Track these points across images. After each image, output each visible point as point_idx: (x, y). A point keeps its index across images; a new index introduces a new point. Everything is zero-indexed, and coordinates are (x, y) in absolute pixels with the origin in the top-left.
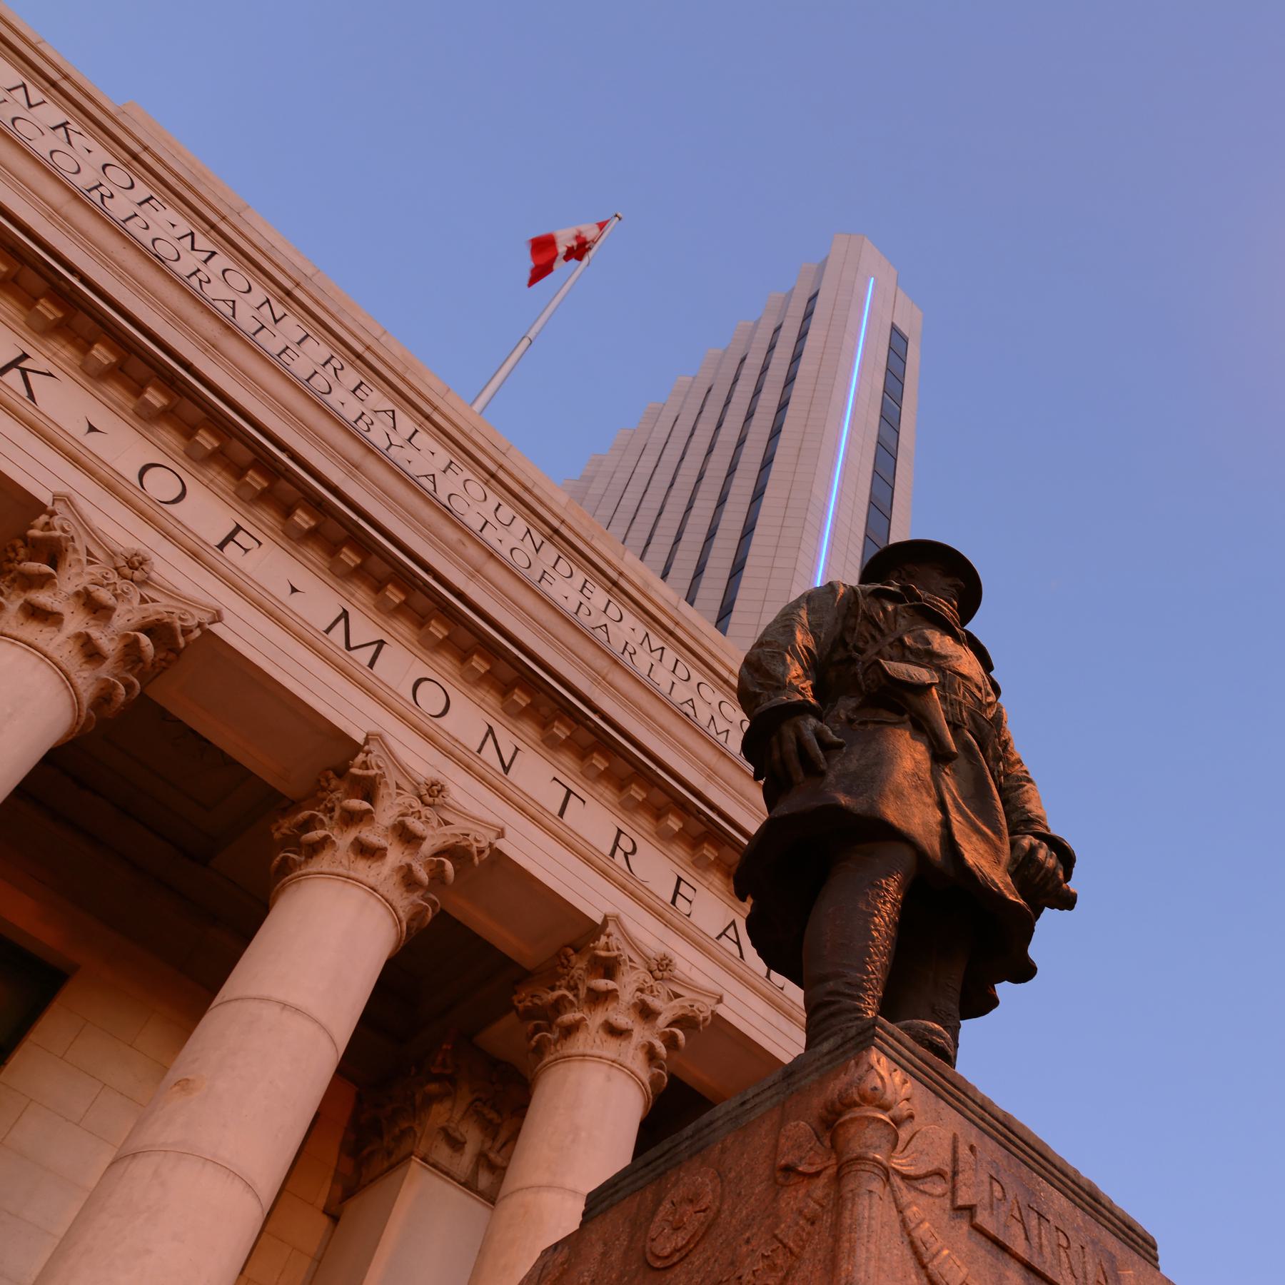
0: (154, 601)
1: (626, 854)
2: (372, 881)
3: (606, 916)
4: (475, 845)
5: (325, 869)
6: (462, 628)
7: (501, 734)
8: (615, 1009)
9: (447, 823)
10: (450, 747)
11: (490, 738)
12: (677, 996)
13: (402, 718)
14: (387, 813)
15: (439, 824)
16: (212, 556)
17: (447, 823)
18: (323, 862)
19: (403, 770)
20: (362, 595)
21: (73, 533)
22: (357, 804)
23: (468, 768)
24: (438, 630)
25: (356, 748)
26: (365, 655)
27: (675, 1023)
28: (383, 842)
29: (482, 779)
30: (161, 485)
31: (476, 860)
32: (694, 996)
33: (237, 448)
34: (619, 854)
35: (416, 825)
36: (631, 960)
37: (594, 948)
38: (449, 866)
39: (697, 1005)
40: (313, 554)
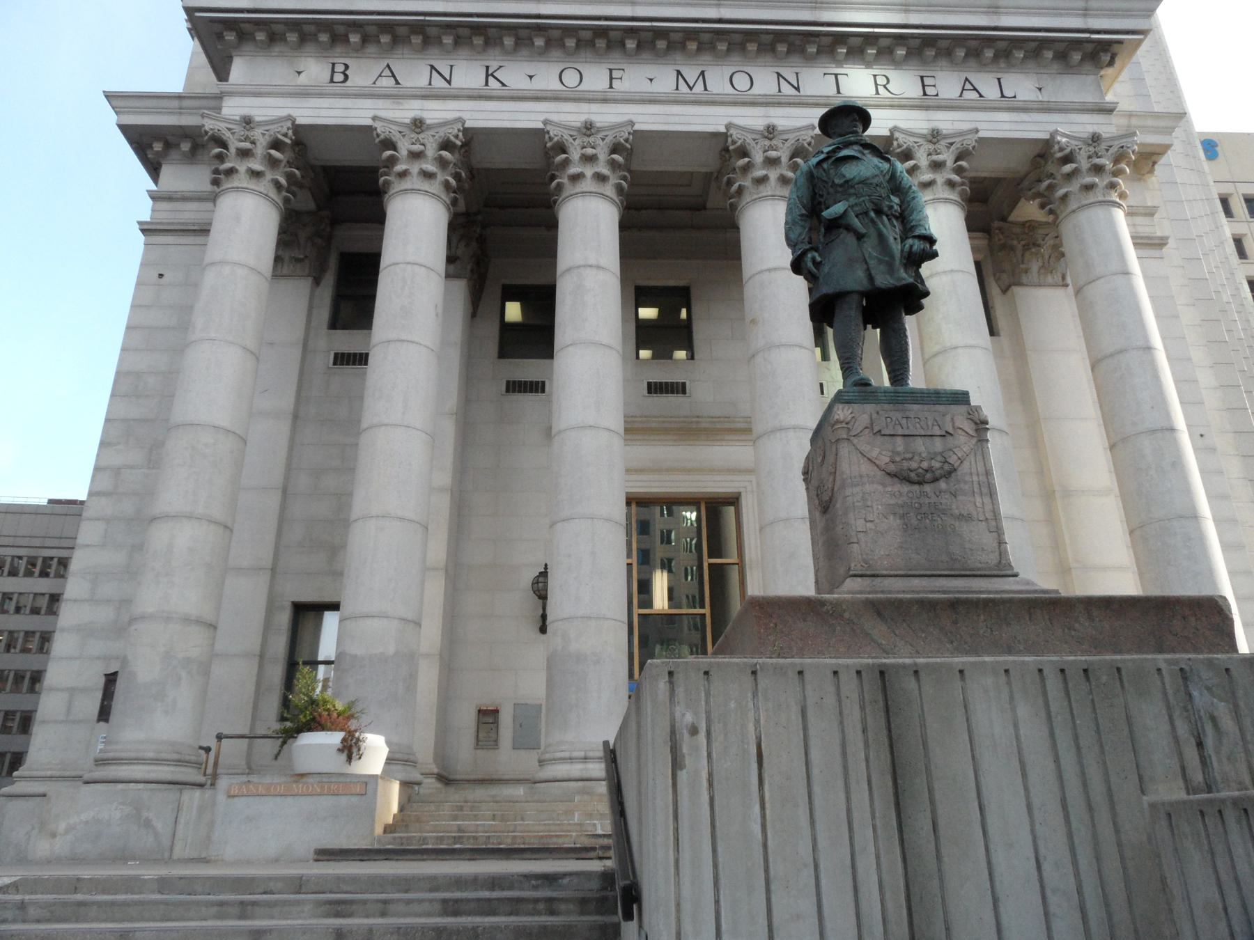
0: (606, 136)
1: (885, 86)
2: (770, 193)
3: (890, 130)
4: (805, 143)
5: (748, 200)
6: (732, 35)
7: (787, 72)
8: (920, 173)
9: (786, 140)
10: (765, 100)
11: (781, 79)
12: (952, 144)
13: (735, 103)
14: (758, 157)
15: (783, 143)
16: (610, 95)
17: (786, 140)
18: (747, 198)
19: (752, 131)
20: (678, 57)
21: (560, 133)
22: (743, 161)
23: (779, 104)
24: (722, 47)
25: (725, 136)
26: (699, 88)
27: (957, 160)
28: (764, 172)
29: (790, 104)
30: (571, 78)
31: (810, 149)
32: (961, 139)
33: (461, 31)
34: (881, 89)
35: (773, 154)
36: (916, 143)
37: (894, 150)
38: (799, 160)
39: (965, 143)
40: (646, 55)
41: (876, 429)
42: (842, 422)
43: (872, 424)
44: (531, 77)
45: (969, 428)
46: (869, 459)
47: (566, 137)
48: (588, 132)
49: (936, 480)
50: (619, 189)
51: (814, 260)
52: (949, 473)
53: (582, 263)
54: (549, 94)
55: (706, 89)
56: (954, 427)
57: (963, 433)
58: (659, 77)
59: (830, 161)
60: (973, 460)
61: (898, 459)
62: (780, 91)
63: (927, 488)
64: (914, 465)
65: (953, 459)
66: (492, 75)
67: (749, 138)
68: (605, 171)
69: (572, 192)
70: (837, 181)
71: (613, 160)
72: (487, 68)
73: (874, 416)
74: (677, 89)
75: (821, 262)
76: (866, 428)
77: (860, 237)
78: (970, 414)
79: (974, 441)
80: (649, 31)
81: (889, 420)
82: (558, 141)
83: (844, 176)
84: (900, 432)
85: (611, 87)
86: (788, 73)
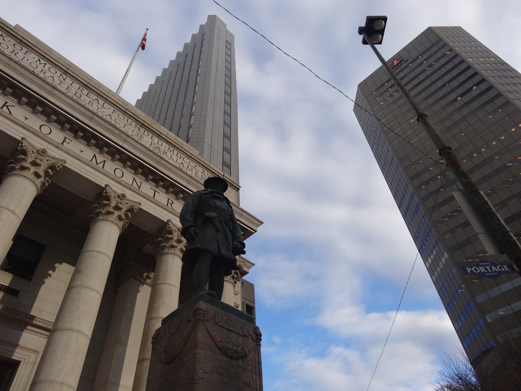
1: (171, 204)
3: (168, 220)
13: (113, 179)
16: (61, 146)
19: (115, 192)
23: (130, 189)
26: (101, 165)
29: (134, 191)
30: (45, 130)
36: (175, 230)
41: (216, 321)
42: (202, 310)
43: (215, 317)
44: (26, 118)
45: (254, 336)
46: (211, 336)
47: (29, 150)
48: (42, 154)
49: (238, 359)
50: (43, 184)
51: (194, 231)
52: (246, 356)
53: (5, 206)
54: (31, 129)
55: (103, 167)
56: (248, 333)
57: (251, 338)
58: (88, 153)
59: (210, 195)
60: (254, 354)
61: (224, 341)
62: (132, 185)
63: (234, 362)
64: (230, 347)
65: (246, 350)
66: (7, 106)
67: (113, 194)
68: (42, 173)
69: (18, 173)
70: (211, 204)
71: (48, 171)
72: (6, 102)
73: (217, 313)
74: (91, 161)
75: (198, 233)
76: (212, 318)
77: (217, 230)
78: (255, 329)
79: (255, 343)
80: (91, 133)
81: (222, 318)
82: (25, 149)
83: (215, 204)
84: (226, 326)
85: (62, 143)
86: (138, 180)
